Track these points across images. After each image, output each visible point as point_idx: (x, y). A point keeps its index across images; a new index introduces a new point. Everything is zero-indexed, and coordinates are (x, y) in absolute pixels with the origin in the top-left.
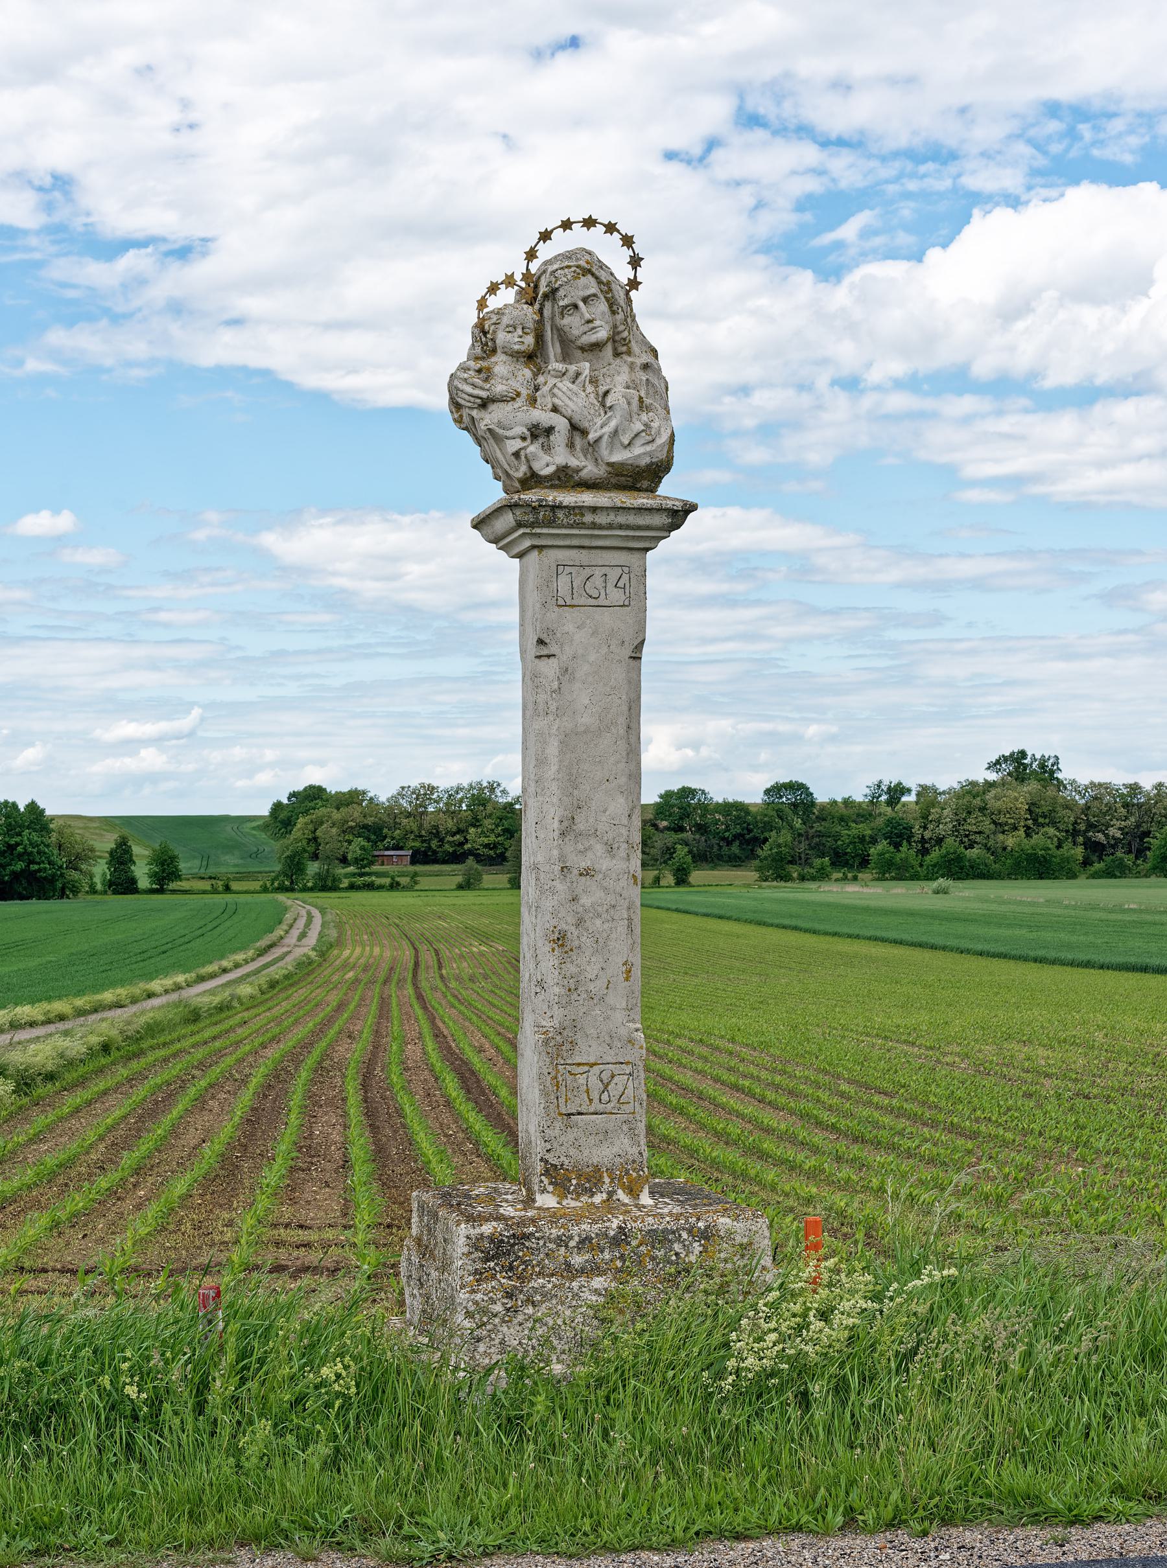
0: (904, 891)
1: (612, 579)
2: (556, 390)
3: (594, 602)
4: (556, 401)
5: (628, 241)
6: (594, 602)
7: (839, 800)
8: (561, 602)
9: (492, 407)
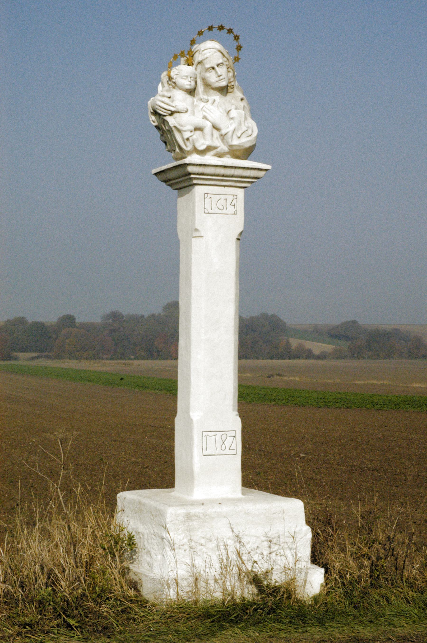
0: (51, 361)
1: (229, 202)
2: (204, 109)
3: (221, 212)
4: (205, 114)
5: (237, 38)
6: (221, 212)
7: (270, 314)
8: (206, 211)
9: (176, 115)
